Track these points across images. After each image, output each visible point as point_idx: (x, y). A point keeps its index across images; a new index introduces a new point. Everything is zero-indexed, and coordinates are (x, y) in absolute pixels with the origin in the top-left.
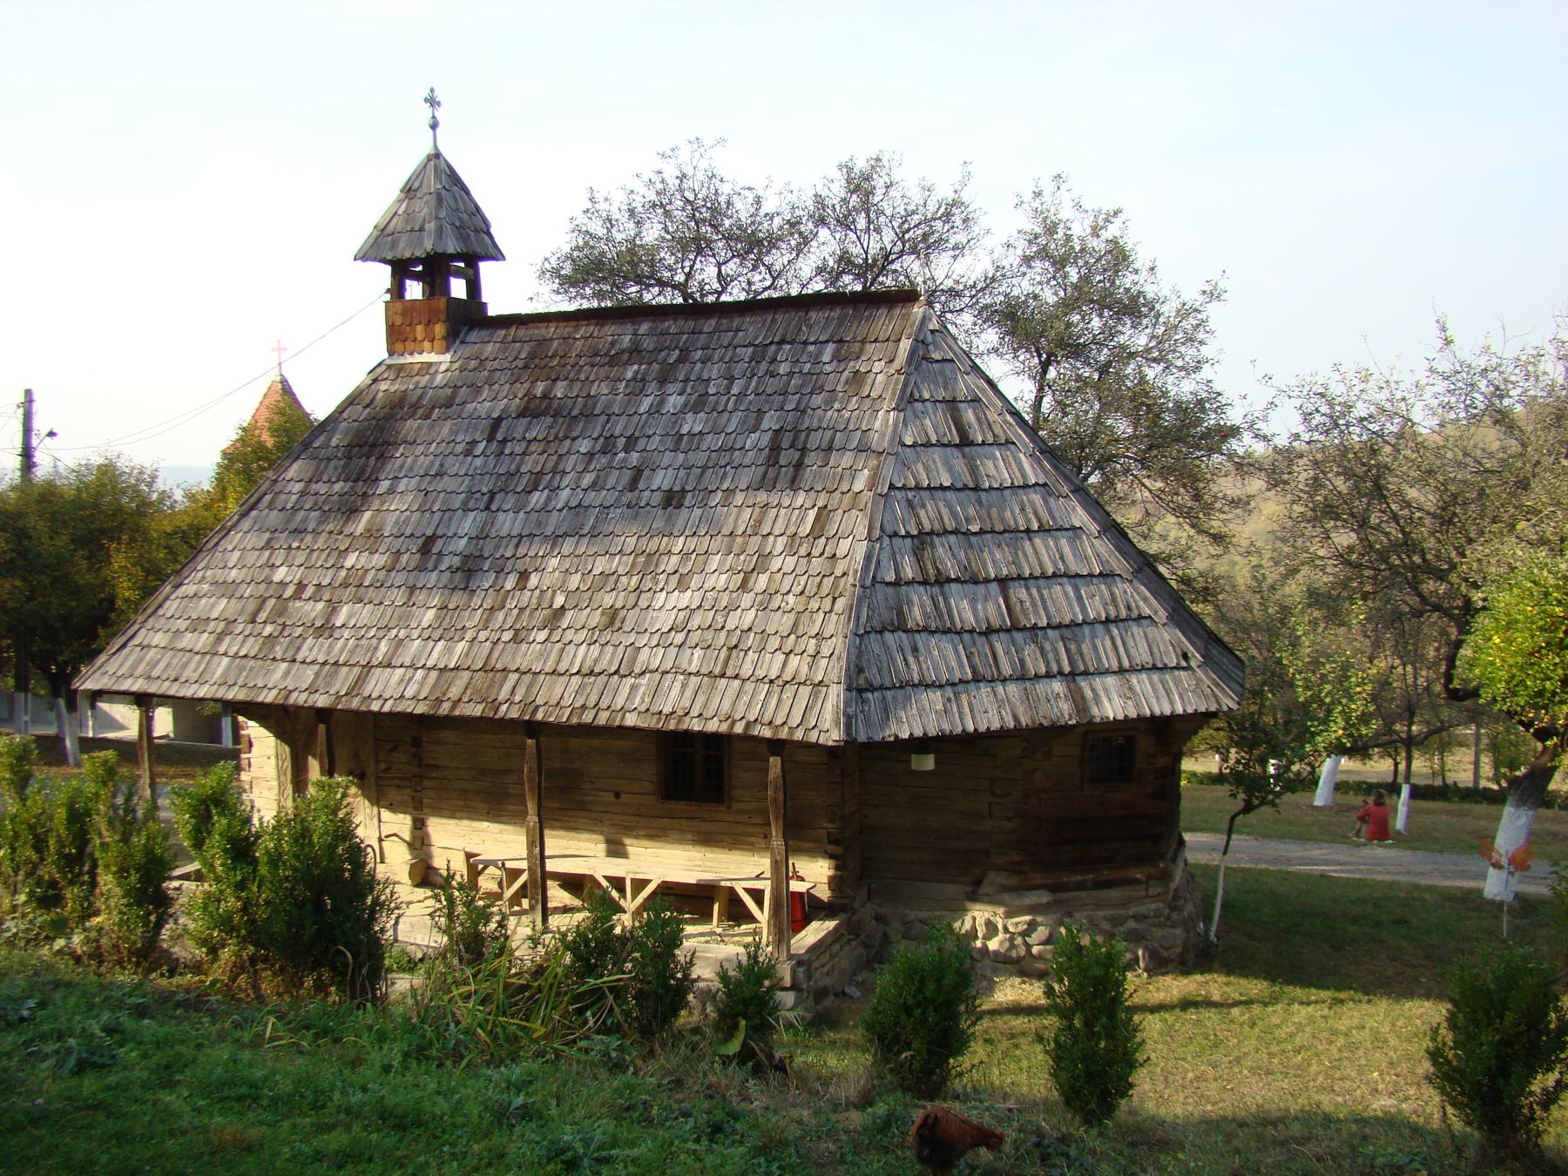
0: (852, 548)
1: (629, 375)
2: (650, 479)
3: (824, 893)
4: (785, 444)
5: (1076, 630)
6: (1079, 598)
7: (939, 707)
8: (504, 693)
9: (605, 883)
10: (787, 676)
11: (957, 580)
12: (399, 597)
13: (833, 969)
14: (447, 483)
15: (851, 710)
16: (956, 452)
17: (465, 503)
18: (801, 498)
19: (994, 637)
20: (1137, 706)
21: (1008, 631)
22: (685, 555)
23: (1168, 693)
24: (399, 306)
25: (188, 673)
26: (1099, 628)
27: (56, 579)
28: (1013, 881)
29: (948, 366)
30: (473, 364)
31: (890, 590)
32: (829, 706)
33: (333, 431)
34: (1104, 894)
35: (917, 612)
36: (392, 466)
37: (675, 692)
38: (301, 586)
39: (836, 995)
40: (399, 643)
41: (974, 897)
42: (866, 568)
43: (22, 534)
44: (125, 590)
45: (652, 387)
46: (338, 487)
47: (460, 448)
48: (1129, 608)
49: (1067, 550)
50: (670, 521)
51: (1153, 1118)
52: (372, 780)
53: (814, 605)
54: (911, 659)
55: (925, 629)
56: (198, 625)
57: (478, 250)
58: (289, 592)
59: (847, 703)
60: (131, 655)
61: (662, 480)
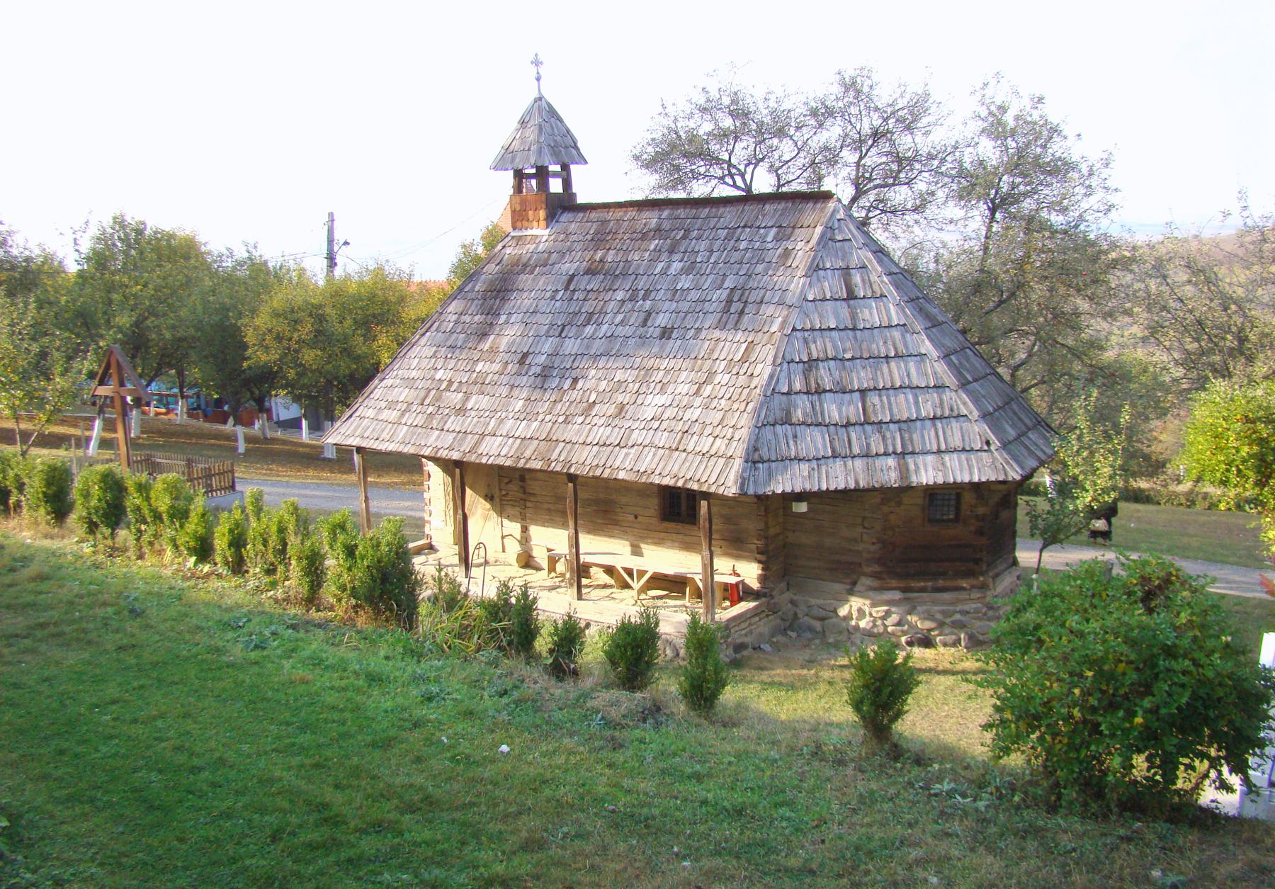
0: (763, 371)
1: (652, 247)
2: (655, 319)
3: (755, 585)
4: (735, 299)
5: (911, 424)
6: (916, 403)
7: (806, 474)
8: (554, 456)
9: (622, 572)
10: (712, 452)
11: (830, 391)
12: (504, 391)
13: (751, 632)
14: (539, 318)
15: (746, 475)
16: (844, 304)
17: (548, 331)
18: (739, 335)
19: (851, 429)
20: (945, 475)
21: (861, 424)
22: (667, 371)
23: (970, 467)
24: (518, 199)
25: (385, 435)
26: (928, 423)
27: (345, 349)
28: (876, 583)
29: (846, 244)
30: (562, 236)
31: (784, 398)
32: (733, 472)
33: (477, 280)
34: (934, 595)
35: (799, 413)
36: (508, 306)
37: (649, 458)
38: (451, 382)
39: (754, 649)
40: (501, 421)
41: (851, 592)
42: (768, 384)
43: (321, 319)
44: (385, 357)
45: (664, 256)
46: (477, 318)
47: (548, 295)
48: (952, 410)
49: (913, 371)
50: (662, 348)
51: (866, 727)
52: (497, 500)
53: (735, 406)
54: (791, 443)
55: (803, 423)
56: (391, 405)
58: (443, 387)
59: (744, 470)
60: (354, 421)
61: (661, 320)
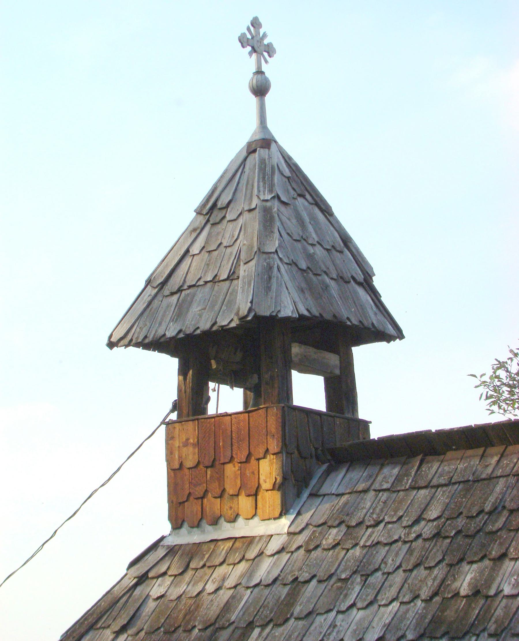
24: (191, 429)
30: (333, 535)
57: (348, 314)
